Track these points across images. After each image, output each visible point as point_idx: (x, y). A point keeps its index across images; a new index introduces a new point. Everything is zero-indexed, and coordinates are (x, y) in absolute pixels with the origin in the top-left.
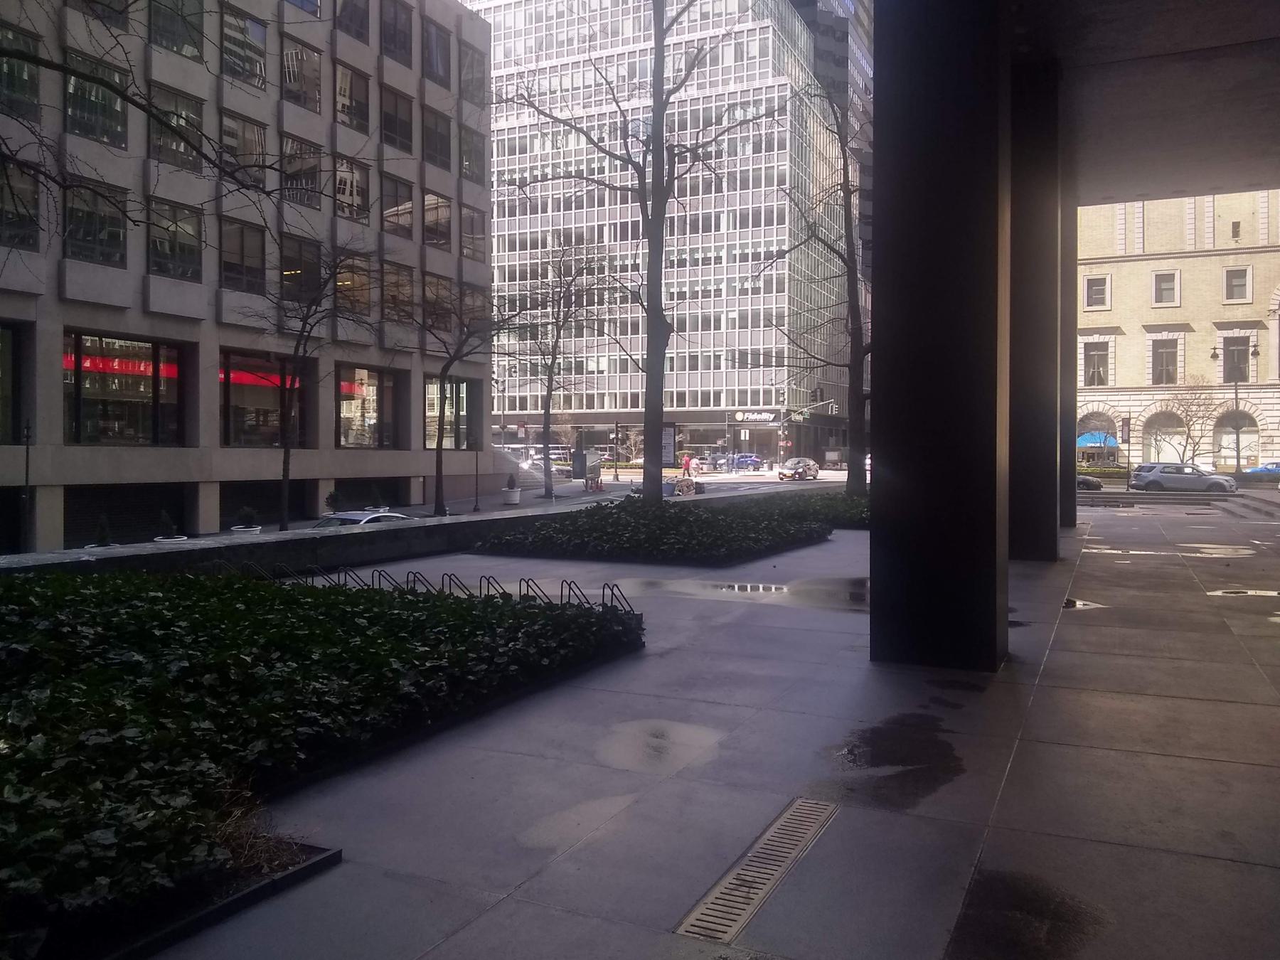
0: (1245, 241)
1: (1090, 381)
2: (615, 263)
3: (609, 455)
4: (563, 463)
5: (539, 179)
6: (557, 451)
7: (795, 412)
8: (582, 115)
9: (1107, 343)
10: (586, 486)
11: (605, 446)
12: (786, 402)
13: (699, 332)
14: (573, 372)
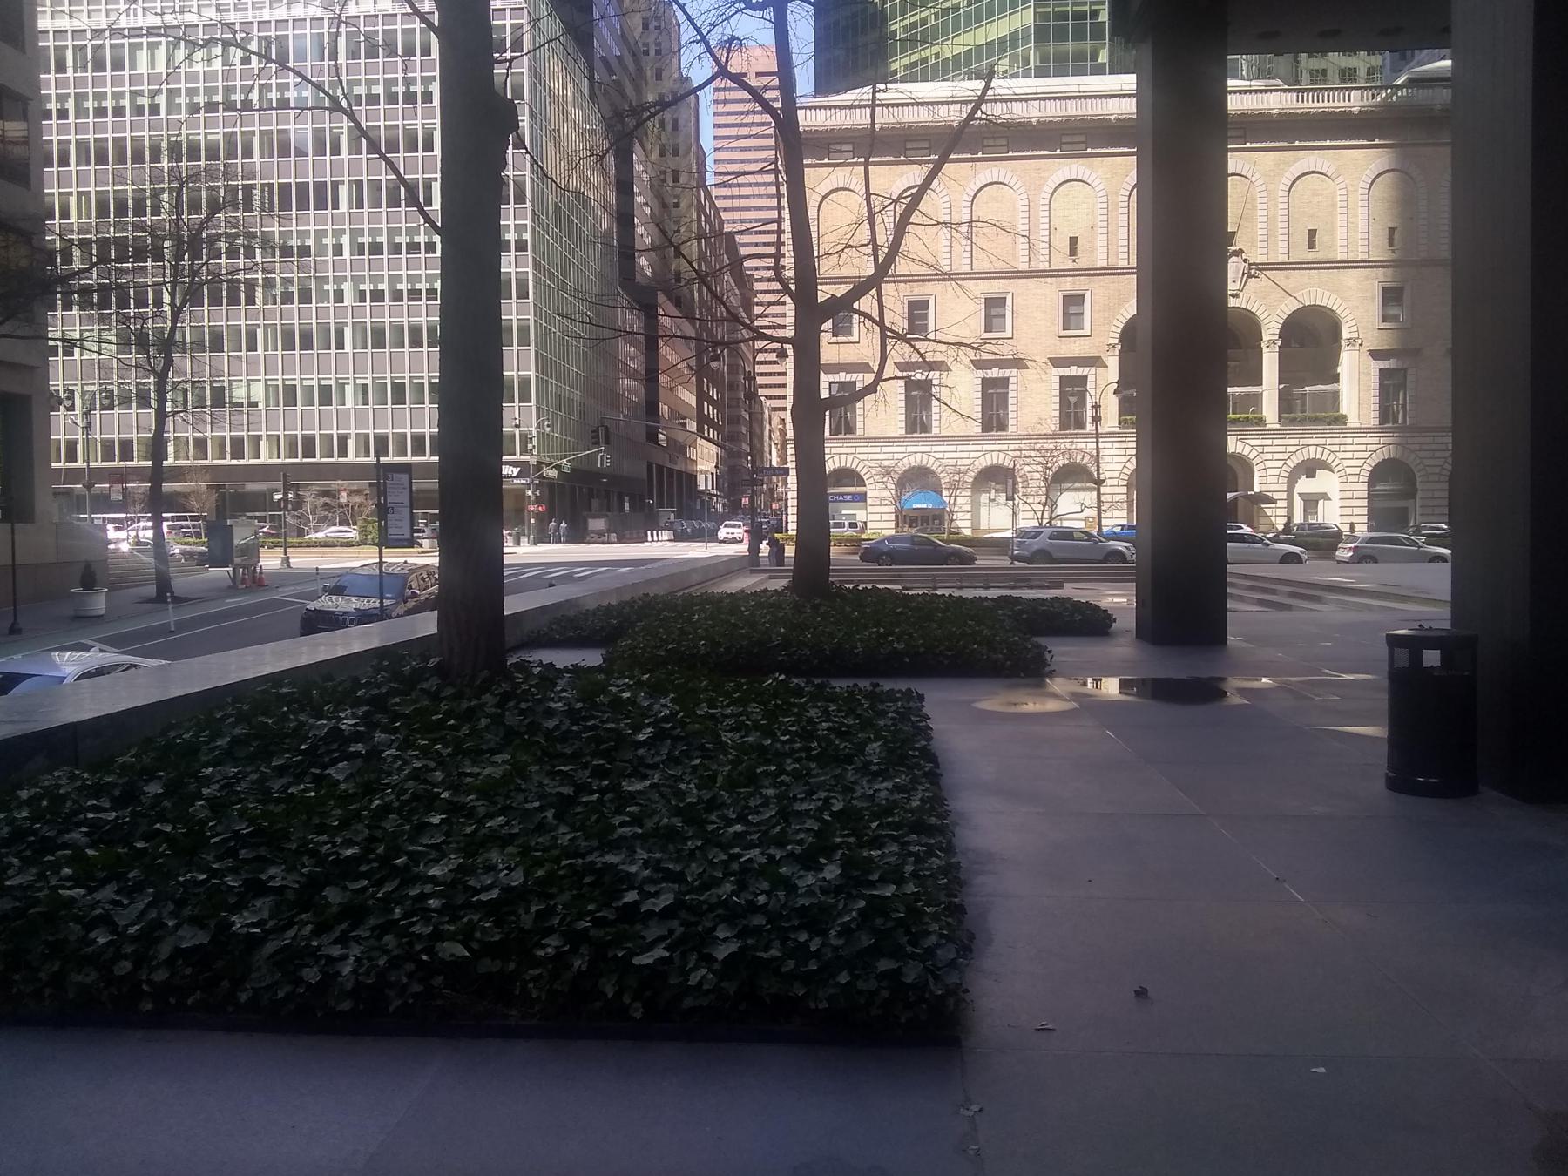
0: (1083, 262)
1: (836, 431)
2: (325, 241)
3: (271, 527)
4: (195, 540)
5: (274, 105)
6: (183, 523)
7: (548, 465)
8: (196, 23)
9: (1086, 377)
10: (234, 579)
11: (263, 514)
12: (535, 452)
13: (406, 349)
14: (134, 405)
